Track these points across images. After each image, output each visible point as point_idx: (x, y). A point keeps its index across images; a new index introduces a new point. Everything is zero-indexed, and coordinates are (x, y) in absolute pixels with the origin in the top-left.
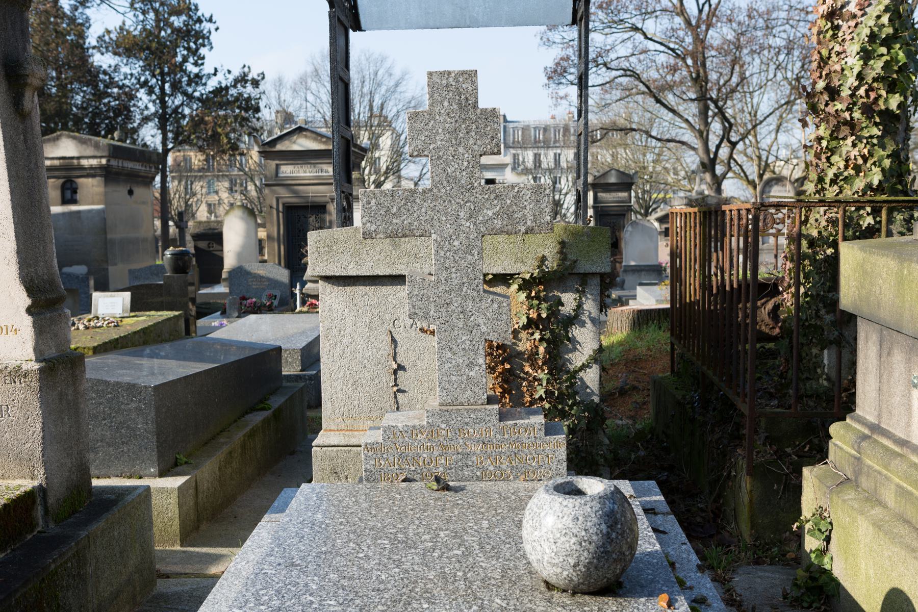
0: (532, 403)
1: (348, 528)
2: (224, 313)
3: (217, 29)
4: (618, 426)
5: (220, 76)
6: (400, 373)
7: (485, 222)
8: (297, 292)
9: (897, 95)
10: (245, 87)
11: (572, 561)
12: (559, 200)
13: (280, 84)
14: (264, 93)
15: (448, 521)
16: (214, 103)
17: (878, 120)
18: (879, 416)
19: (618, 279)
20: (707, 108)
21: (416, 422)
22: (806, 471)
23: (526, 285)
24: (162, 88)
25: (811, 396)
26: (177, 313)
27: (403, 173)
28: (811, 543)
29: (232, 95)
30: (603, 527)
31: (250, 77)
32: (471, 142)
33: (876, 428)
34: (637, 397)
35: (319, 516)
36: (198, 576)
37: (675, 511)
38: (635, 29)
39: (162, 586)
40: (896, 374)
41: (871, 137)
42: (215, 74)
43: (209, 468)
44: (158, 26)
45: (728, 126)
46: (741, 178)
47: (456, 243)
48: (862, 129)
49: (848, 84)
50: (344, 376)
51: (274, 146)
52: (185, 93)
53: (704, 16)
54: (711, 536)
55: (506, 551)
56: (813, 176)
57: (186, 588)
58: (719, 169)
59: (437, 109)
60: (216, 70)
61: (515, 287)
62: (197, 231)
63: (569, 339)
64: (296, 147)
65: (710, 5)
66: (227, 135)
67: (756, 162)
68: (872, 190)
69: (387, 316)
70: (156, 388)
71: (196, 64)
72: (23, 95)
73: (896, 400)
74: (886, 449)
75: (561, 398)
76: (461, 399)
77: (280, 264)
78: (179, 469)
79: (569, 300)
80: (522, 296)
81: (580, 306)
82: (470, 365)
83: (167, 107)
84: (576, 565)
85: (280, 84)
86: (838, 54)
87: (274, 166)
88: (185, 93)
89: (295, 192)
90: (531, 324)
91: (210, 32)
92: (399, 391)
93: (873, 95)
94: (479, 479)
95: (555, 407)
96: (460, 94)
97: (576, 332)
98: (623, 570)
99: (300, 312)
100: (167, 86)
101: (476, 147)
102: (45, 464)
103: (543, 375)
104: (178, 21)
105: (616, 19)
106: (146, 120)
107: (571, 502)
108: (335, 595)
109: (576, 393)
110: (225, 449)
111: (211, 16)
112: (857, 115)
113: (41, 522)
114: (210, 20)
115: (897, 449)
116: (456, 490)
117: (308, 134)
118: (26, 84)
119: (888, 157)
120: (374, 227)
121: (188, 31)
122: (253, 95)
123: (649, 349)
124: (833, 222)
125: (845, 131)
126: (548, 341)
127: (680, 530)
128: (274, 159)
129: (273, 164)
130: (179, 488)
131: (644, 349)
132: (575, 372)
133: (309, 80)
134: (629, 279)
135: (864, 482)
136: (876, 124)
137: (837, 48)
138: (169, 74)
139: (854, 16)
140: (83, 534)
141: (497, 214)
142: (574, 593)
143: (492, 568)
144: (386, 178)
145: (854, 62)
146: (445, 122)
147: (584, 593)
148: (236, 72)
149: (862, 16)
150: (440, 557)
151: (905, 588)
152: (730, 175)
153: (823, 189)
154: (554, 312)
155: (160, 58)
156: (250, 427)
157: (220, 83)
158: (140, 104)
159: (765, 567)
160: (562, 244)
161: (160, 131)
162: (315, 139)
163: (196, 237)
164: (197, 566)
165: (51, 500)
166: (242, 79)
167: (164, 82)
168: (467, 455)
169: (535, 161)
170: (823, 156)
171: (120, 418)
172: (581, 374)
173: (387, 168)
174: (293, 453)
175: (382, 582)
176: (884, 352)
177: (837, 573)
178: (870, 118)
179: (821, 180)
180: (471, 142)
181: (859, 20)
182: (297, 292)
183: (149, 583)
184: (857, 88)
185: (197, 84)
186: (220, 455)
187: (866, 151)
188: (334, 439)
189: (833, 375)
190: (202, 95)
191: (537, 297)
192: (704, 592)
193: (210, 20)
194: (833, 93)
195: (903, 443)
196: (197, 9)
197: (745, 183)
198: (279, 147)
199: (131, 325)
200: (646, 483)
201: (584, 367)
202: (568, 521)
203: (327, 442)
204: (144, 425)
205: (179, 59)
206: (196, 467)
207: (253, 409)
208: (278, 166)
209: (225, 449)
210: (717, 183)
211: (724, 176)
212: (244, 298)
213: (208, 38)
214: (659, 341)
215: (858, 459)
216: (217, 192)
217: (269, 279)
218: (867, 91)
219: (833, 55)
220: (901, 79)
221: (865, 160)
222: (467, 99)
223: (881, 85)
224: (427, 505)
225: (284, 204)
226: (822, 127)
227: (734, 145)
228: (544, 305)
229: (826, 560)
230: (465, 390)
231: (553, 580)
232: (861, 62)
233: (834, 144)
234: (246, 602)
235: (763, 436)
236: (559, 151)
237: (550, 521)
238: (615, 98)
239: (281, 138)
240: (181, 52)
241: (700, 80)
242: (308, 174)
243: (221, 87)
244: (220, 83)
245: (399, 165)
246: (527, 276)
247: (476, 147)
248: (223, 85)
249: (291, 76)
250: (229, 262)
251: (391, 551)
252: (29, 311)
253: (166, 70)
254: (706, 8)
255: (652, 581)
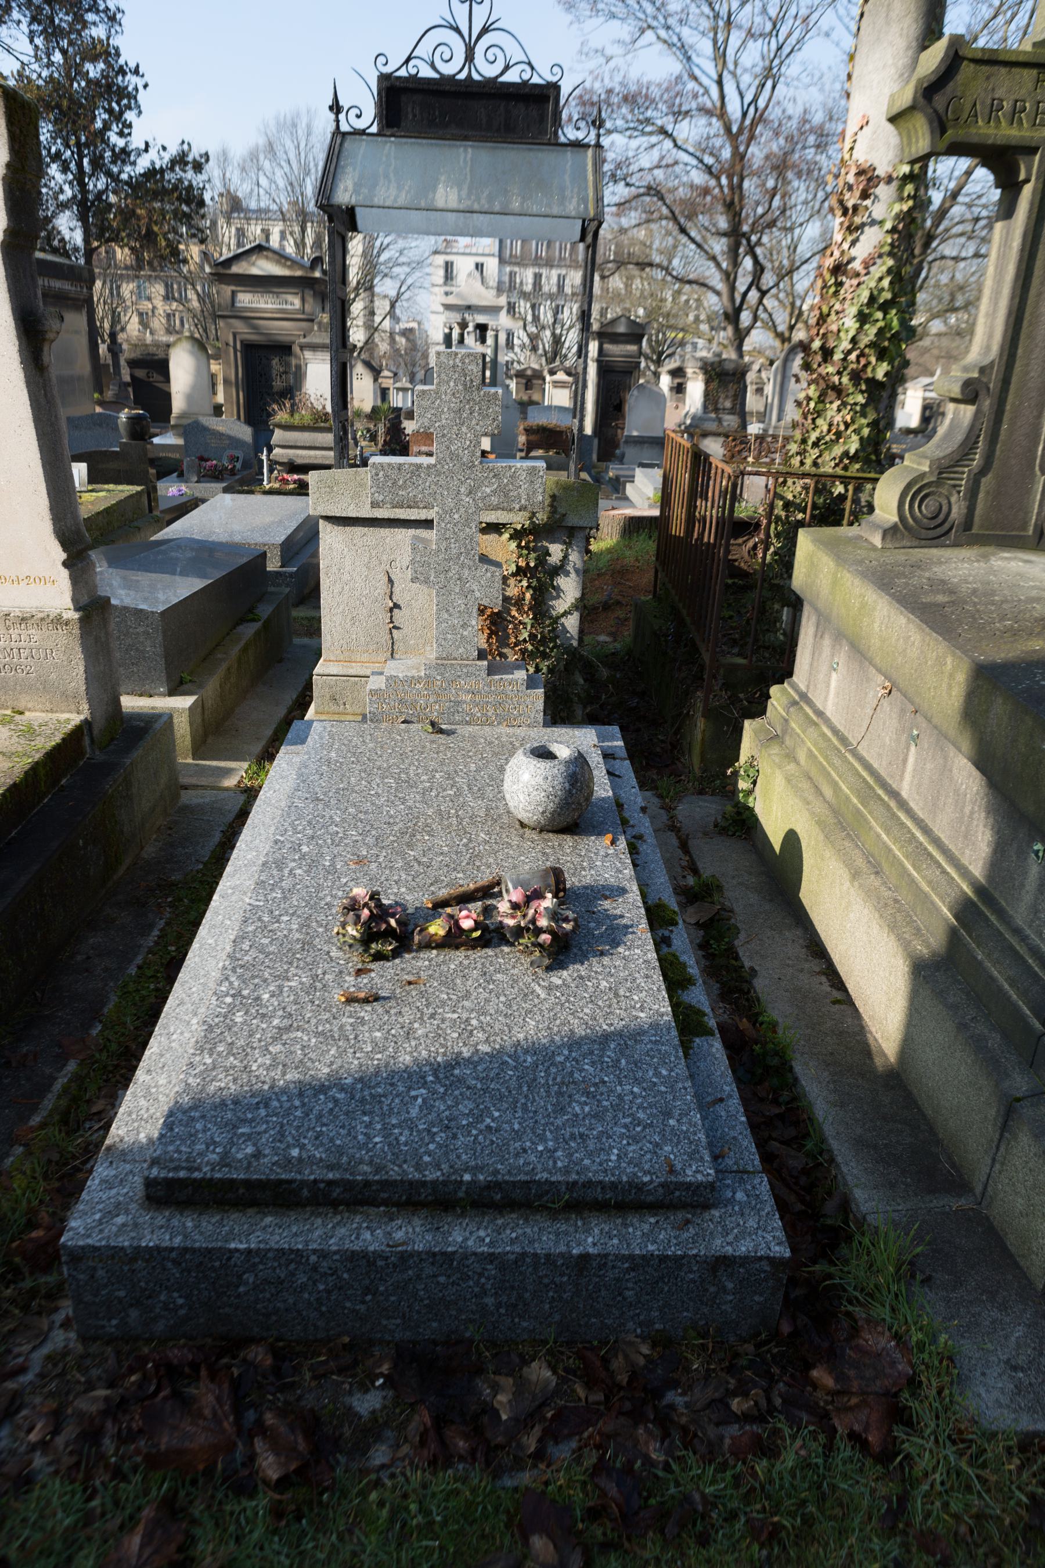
0: (516, 645)
1: (359, 767)
2: (181, 475)
3: (146, 86)
4: (598, 643)
5: (152, 154)
6: (396, 611)
7: (484, 498)
8: (264, 458)
9: (885, 364)
10: (185, 171)
11: (541, 809)
12: (561, 335)
13: (225, 160)
14: (209, 181)
15: (442, 763)
16: (147, 191)
17: (864, 387)
18: (808, 687)
19: (618, 451)
20: (738, 245)
21: (414, 673)
22: (747, 723)
23: (516, 535)
24: (80, 165)
25: (768, 648)
26: (139, 488)
27: (377, 290)
28: (743, 785)
29: (169, 181)
30: (567, 785)
31: (190, 158)
32: (474, 422)
33: (804, 696)
34: (620, 613)
35: (333, 754)
36: (213, 788)
37: (631, 757)
38: (663, 131)
39: (187, 798)
40: (824, 655)
41: (856, 404)
42: (146, 150)
43: (212, 685)
44: (68, 75)
45: (759, 269)
46: (769, 329)
47: (456, 516)
48: (848, 395)
49: (841, 348)
50: (343, 612)
51: (229, 267)
52: (109, 174)
53: (748, 122)
54: (667, 766)
55: (489, 792)
56: (798, 435)
57: (207, 800)
58: (745, 317)
59: (443, 389)
60: (147, 144)
61: (506, 536)
62: (133, 356)
63: (554, 588)
64: (255, 271)
65: (756, 109)
66: (165, 235)
67: (788, 310)
68: (849, 458)
69: (384, 557)
70: (163, 613)
71: (121, 134)
72: (41, 350)
73: (821, 676)
74: (807, 715)
75: (543, 641)
76: (455, 655)
77: (239, 418)
78: (185, 687)
79: (556, 551)
80: (513, 545)
81: (566, 557)
82: (464, 626)
83: (88, 191)
84: (543, 813)
85: (225, 160)
86: (837, 313)
87: (229, 293)
88: (109, 174)
89: (255, 327)
90: (520, 572)
91: (136, 89)
92: (395, 627)
93: (863, 361)
94: (468, 723)
95: (537, 649)
96: (465, 375)
97: (561, 581)
98: (579, 817)
99: (271, 492)
100: (86, 161)
101: (478, 428)
102: (90, 701)
103: (528, 619)
104: (94, 70)
105: (641, 117)
106: (63, 206)
107: (543, 765)
108: (356, 827)
109: (557, 637)
110: (224, 666)
111: (138, 66)
112: (845, 380)
113: (88, 749)
114: (136, 72)
115: (815, 718)
116: (448, 733)
117: (270, 254)
118: (44, 340)
119: (868, 425)
120: (381, 498)
121: (109, 86)
122: (194, 183)
123: (637, 560)
124: (806, 488)
125: (832, 395)
126: (534, 589)
127: (633, 775)
128: (228, 284)
129: (227, 290)
130: (190, 708)
131: (632, 559)
132: (558, 618)
133: (262, 157)
134: (630, 452)
135: (788, 741)
136: (862, 392)
137: (838, 307)
138: (87, 145)
139: (858, 275)
140: (128, 761)
141: (494, 492)
142: (541, 831)
143: (478, 807)
144: (357, 295)
145: (850, 323)
146: (450, 401)
147: (549, 831)
148: (173, 150)
149: (866, 274)
150: (437, 796)
151: (798, 831)
152: (758, 324)
153: (805, 451)
154: (541, 561)
155: (74, 122)
156: (243, 643)
157: (153, 163)
158: (53, 184)
159: (707, 797)
160: (553, 497)
161: (79, 224)
162: (278, 262)
163: (133, 364)
164: (211, 779)
165: (96, 732)
166: (180, 160)
167: (81, 156)
168: (458, 703)
169: (534, 284)
170: (810, 417)
171: (129, 641)
172: (563, 620)
173: (358, 283)
174: (280, 661)
175: (391, 817)
176: (819, 635)
177: (758, 810)
178: (856, 385)
179: (804, 441)
180: (474, 422)
181: (862, 279)
182: (264, 458)
183: (176, 797)
184: (849, 352)
185: (124, 162)
186: (221, 671)
187: (848, 418)
188: (334, 669)
189: (788, 631)
190: (131, 177)
191: (527, 547)
192: (642, 830)
193: (136, 72)
194: (827, 353)
195: (820, 714)
196: (118, 54)
197: (771, 335)
198: (236, 269)
199: (92, 503)
200: (610, 728)
201: (565, 614)
202: (540, 780)
203: (327, 672)
204: (153, 648)
205: (99, 124)
206: (201, 686)
207: (242, 620)
208: (234, 293)
209: (224, 666)
210: (740, 336)
211: (748, 330)
212: (202, 459)
213: (135, 98)
214: (647, 552)
215: (786, 721)
216: (149, 299)
217: (229, 437)
218: (858, 357)
219: (833, 313)
220: (892, 347)
221: (847, 426)
222: (472, 381)
223: (872, 351)
224: (424, 747)
225: (242, 342)
226: (813, 387)
227: (763, 293)
228: (533, 555)
229: (751, 799)
230: (459, 647)
231: (526, 821)
232: (857, 325)
233: (820, 406)
234: (286, 830)
235: (721, 682)
236: (563, 272)
237: (526, 777)
238: (634, 222)
239: (237, 258)
240: (101, 117)
241: (733, 207)
242: (270, 306)
243: (154, 168)
244: (153, 163)
245: (372, 280)
246: (519, 527)
247: (478, 428)
248: (157, 167)
249: (238, 151)
250: (178, 404)
251: (396, 790)
252: (65, 564)
253: (83, 138)
254: (752, 110)
255: (602, 823)
